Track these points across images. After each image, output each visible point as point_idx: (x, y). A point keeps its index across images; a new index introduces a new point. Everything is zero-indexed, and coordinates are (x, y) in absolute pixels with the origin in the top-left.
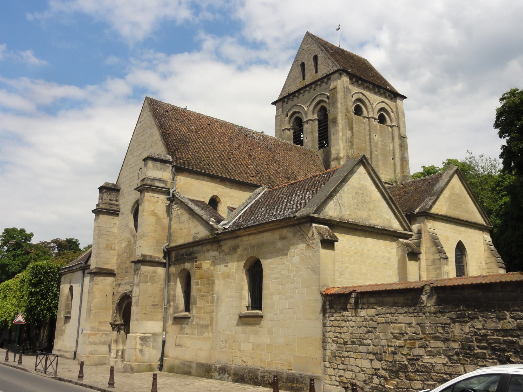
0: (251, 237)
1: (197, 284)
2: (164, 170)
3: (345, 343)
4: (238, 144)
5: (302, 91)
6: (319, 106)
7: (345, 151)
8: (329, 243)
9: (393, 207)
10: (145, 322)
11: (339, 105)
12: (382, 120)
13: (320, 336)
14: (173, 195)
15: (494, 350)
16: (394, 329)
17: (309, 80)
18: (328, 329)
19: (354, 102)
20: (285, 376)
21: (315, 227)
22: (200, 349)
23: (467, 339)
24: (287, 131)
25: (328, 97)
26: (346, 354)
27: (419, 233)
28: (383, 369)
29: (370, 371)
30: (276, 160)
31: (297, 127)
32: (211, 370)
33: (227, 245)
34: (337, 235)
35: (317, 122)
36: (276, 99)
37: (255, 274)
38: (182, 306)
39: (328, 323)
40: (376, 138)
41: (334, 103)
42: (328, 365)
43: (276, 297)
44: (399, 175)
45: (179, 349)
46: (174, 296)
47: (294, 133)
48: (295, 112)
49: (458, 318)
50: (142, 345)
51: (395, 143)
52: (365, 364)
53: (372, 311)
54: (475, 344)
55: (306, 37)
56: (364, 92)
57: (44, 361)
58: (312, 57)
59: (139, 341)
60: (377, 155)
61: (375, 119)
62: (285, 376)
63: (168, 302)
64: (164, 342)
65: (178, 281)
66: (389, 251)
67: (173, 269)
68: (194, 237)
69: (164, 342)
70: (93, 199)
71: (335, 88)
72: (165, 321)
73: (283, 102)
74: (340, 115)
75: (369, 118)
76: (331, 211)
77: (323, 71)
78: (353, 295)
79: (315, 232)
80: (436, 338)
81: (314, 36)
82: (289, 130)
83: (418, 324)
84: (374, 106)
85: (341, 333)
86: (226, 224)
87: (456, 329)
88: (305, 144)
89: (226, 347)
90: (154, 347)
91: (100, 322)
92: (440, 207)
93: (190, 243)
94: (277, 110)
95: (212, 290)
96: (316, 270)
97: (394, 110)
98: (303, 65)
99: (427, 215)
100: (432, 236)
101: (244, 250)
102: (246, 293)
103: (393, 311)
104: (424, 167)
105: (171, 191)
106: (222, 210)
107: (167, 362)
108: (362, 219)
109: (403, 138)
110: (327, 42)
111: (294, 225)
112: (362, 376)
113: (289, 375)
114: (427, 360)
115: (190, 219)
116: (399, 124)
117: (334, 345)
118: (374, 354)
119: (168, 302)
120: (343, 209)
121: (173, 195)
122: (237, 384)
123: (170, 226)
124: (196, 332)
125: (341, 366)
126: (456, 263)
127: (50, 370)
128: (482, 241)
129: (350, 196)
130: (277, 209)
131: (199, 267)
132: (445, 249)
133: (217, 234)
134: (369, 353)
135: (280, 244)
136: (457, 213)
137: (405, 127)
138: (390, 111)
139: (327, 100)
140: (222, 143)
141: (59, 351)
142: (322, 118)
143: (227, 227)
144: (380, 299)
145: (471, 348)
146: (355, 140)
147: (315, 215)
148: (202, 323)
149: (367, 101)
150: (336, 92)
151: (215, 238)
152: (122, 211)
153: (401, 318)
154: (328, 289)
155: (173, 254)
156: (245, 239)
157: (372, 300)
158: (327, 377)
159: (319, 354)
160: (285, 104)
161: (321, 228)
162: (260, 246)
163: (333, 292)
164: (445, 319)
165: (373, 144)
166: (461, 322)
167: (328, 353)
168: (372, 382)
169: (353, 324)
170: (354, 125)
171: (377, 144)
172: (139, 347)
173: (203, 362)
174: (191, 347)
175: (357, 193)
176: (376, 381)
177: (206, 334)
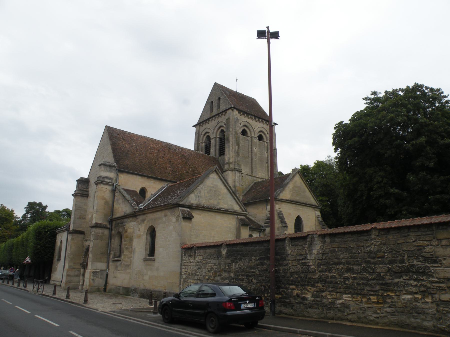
0: (151, 215)
1: (125, 241)
2: (111, 172)
4: (163, 154)
5: (211, 120)
6: (220, 129)
7: (233, 158)
8: (188, 218)
9: (235, 197)
12: (260, 138)
13: (179, 271)
14: (116, 187)
17: (215, 112)
23: (237, 271)
25: (225, 124)
30: (188, 164)
31: (208, 142)
33: (141, 218)
34: (193, 214)
36: (196, 123)
40: (255, 150)
43: (161, 249)
48: (206, 133)
56: (250, 121)
57: (37, 286)
58: (217, 98)
61: (255, 138)
63: (110, 251)
64: (107, 275)
70: (73, 187)
72: (108, 262)
73: (200, 126)
74: (231, 135)
75: (251, 137)
76: (192, 199)
79: (180, 213)
80: (225, 271)
90: (101, 278)
91: (74, 263)
92: (286, 194)
93: (122, 217)
95: (132, 245)
98: (212, 102)
101: (148, 221)
104: (301, 165)
105: (115, 184)
106: (148, 195)
107: (109, 287)
111: (171, 208)
115: (123, 202)
120: (201, 199)
121: (116, 187)
122: (141, 299)
123: (113, 206)
127: (40, 290)
128: (314, 215)
129: (206, 191)
135: (164, 219)
136: (298, 198)
138: (266, 133)
139: (224, 126)
140: (152, 154)
141: (54, 281)
142: (222, 137)
144: (205, 250)
148: (126, 264)
149: (250, 127)
152: (90, 195)
155: (114, 223)
156: (148, 215)
159: (178, 282)
160: (201, 127)
161: (184, 210)
164: (229, 261)
165: (253, 154)
171: (256, 154)
173: (126, 286)
175: (211, 190)
177: (128, 271)
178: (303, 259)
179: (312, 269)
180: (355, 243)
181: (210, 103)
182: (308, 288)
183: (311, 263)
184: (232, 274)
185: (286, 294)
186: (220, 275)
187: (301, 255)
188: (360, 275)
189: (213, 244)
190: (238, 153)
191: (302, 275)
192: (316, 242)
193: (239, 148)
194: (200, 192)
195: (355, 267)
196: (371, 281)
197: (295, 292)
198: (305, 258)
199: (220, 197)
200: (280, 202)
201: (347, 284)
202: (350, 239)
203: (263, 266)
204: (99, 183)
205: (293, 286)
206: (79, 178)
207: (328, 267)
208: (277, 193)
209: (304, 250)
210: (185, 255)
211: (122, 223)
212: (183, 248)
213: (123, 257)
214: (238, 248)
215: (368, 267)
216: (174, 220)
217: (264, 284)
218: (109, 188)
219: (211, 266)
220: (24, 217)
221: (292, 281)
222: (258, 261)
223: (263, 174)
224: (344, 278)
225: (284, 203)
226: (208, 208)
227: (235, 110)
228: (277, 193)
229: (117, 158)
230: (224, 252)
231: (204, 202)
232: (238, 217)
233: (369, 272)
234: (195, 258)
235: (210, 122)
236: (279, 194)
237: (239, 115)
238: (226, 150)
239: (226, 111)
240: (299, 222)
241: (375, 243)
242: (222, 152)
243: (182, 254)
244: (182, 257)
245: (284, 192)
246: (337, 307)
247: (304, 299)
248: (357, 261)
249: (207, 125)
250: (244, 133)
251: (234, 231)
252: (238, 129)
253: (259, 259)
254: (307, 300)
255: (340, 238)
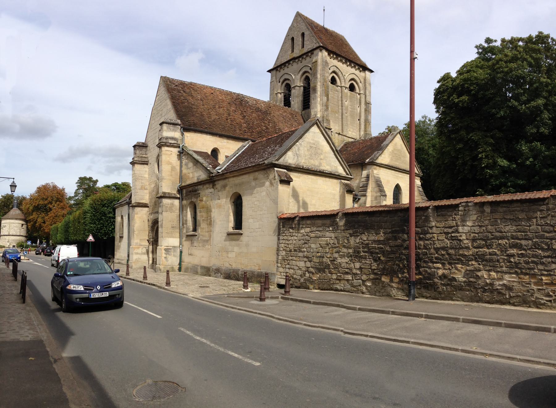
0: (235, 179)
1: (201, 212)
2: (175, 131)
3: (290, 251)
8: (287, 181)
10: (167, 239)
11: (319, 76)
12: (352, 88)
13: (276, 246)
15: (372, 253)
16: (321, 241)
17: (297, 53)
18: (281, 241)
19: (331, 73)
20: (256, 273)
21: (277, 171)
22: (203, 257)
24: (279, 95)
25: (311, 69)
26: (291, 258)
27: (368, 177)
28: (312, 267)
29: (304, 269)
30: (268, 119)
31: (287, 92)
32: (209, 270)
33: (219, 184)
35: (302, 88)
36: (271, 67)
37: (238, 203)
38: (191, 228)
39: (281, 238)
41: (315, 74)
42: (279, 265)
43: (251, 221)
44: (362, 133)
45: (191, 257)
46: (186, 221)
47: (284, 96)
48: (285, 80)
49: (353, 233)
50: (166, 254)
51: (362, 108)
52: (302, 264)
53: (308, 230)
54: (361, 249)
55: (296, 16)
56: (340, 65)
58: (300, 34)
59: (164, 252)
60: (347, 117)
61: (346, 88)
62: (256, 273)
65: (189, 210)
66: (333, 188)
67: (184, 202)
68: (198, 179)
69: (181, 252)
71: (316, 62)
72: (181, 237)
73: (277, 70)
74: (319, 84)
75: (341, 87)
76: (290, 158)
77: (309, 46)
78: (297, 219)
79: (276, 175)
80: (344, 247)
81: (303, 16)
82: (281, 93)
83: (336, 238)
84: (345, 77)
85: (288, 244)
86: (220, 169)
87: (352, 240)
88: (292, 106)
89: (219, 255)
90: (174, 256)
91: (140, 240)
92: (384, 158)
94: (272, 77)
96: (275, 201)
97: (362, 80)
99: (373, 163)
100: (377, 179)
102: (232, 218)
103: (321, 229)
105: (181, 146)
106: (221, 159)
108: (314, 165)
109: (368, 104)
110: (314, 22)
111: (264, 169)
112: (300, 272)
113: (258, 273)
114: (339, 260)
116: (365, 92)
117: (284, 252)
118: (307, 257)
119: (183, 225)
120: (300, 158)
121: (183, 149)
122: (225, 280)
124: (201, 245)
125: (287, 266)
126: (394, 199)
129: (306, 149)
130: (254, 158)
131: (202, 200)
132: (385, 189)
133: (212, 176)
134: (304, 257)
135: (253, 183)
136: (397, 164)
137: (370, 95)
138: (359, 82)
139: (310, 71)
142: (306, 85)
143: (220, 171)
144: (313, 221)
145: (359, 252)
146: (330, 105)
147: (277, 162)
149: (340, 73)
150: (317, 65)
151: (211, 179)
153: (328, 234)
154: (283, 214)
155: (184, 191)
156: (231, 179)
157: (309, 222)
158: (279, 273)
159: (274, 258)
160: (278, 72)
162: (241, 184)
163: (285, 216)
165: (344, 108)
166: (355, 236)
167: (280, 258)
168: (305, 276)
169: (296, 238)
170: (330, 92)
171: (347, 109)
172: (164, 255)
173: (205, 265)
174: (199, 256)
175: (311, 147)
176: (307, 275)
177: (207, 246)
178: (453, 232)
179: (465, 244)
180: (525, 213)
181: (291, 40)
182: (459, 266)
183: (464, 237)
184: (351, 251)
185: (429, 274)
186: (338, 252)
187: (451, 227)
188: (530, 252)
189: (314, 214)
190: (327, 106)
191: (452, 251)
192: (471, 212)
193: (328, 100)
194: (299, 149)
195: (523, 242)
196: (545, 259)
197: (440, 272)
198: (457, 231)
199: (322, 157)
200: (378, 168)
201: (512, 262)
202: (518, 209)
203: (397, 240)
204: (163, 145)
205: (438, 265)
206: (83, 176)
207: (486, 242)
208: (375, 156)
209: (454, 222)
210: (283, 227)
211: (196, 191)
212: (280, 219)
213: (199, 230)
214: (360, 218)
215: (542, 242)
216: (267, 183)
217: (397, 262)
218: (175, 151)
219: (327, 241)
220: (76, 193)
221: (436, 258)
222: (390, 235)
223: (353, 133)
224: (507, 255)
225: (382, 169)
226: (308, 170)
227: (324, 51)
228: (375, 156)
229: (179, 113)
230: (342, 223)
231: (304, 162)
232: (343, 181)
233: (543, 249)
234: (298, 230)
235: (290, 65)
236: (378, 158)
237: (328, 58)
238: (312, 102)
239: (312, 51)
240: (397, 190)
241: (553, 214)
242: (306, 104)
243: (279, 224)
244: (279, 229)
245: (383, 155)
246: (497, 289)
247: (454, 279)
248: (527, 235)
249: (286, 70)
250: (333, 81)
251: (338, 198)
252: (327, 75)
253: (390, 232)
254: (456, 281)
255: (505, 207)
